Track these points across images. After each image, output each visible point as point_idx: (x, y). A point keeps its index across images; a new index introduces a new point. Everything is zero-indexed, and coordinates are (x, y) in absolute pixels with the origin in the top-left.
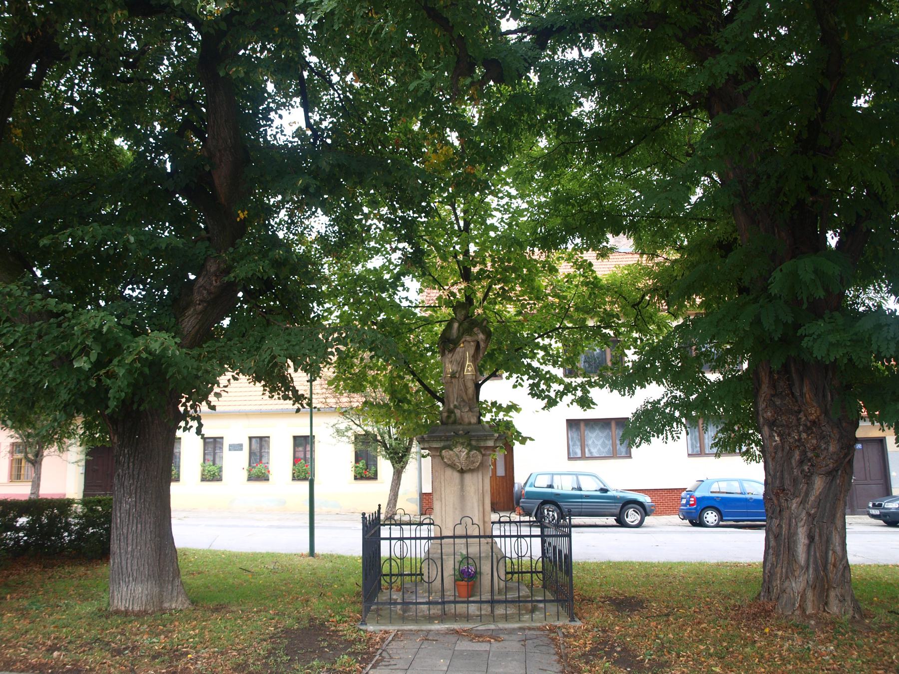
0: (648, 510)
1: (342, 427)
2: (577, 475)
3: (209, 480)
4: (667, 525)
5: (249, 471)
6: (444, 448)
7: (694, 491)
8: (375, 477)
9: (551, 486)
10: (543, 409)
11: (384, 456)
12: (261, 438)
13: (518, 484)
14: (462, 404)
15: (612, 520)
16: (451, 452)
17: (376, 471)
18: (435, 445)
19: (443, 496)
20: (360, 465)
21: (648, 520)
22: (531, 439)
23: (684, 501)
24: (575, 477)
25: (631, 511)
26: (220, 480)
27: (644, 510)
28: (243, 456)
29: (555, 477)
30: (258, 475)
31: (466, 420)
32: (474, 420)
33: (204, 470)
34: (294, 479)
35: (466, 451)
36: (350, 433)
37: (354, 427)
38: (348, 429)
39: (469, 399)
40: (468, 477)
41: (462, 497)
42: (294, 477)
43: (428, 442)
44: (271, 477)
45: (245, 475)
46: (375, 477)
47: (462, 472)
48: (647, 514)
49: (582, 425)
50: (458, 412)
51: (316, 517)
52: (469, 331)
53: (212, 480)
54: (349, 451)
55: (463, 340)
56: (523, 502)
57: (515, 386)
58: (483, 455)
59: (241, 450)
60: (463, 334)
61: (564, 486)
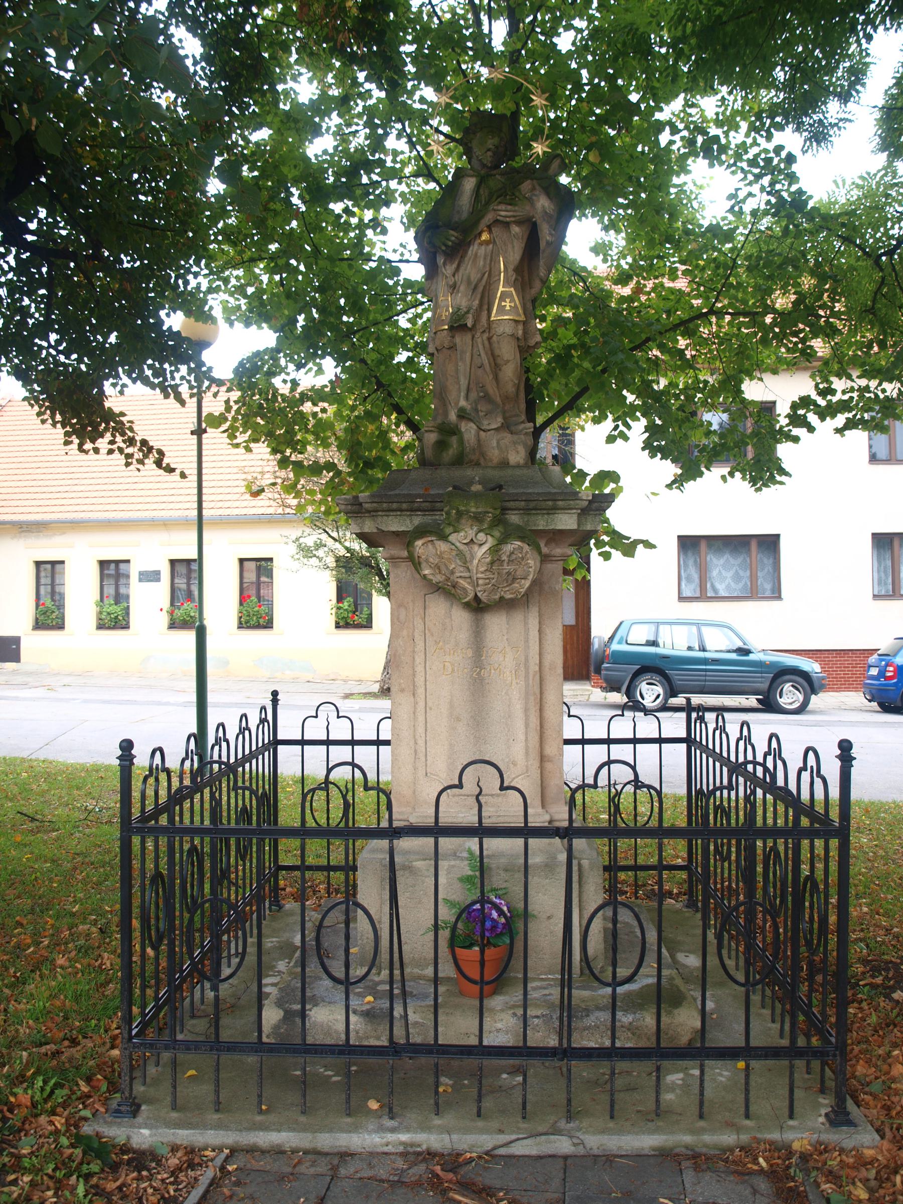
0: (816, 684)
1: (310, 541)
2: (698, 625)
3: (109, 628)
4: (840, 709)
5: (171, 613)
6: (420, 532)
7: (895, 655)
8: (367, 624)
9: (654, 643)
10: (669, 486)
11: (379, 592)
13: (600, 638)
14: (483, 407)
15: (752, 701)
16: (442, 546)
17: (371, 614)
18: (396, 524)
19: (420, 680)
20: (345, 605)
21: (815, 701)
22: (648, 545)
23: (874, 672)
24: (694, 628)
25: (787, 687)
26: (126, 627)
27: (810, 685)
28: (162, 589)
29: (661, 627)
30: (114, 619)
31: (494, 454)
32: (517, 456)
33: (101, 613)
34: (240, 626)
35: (491, 542)
36: (321, 553)
37: (330, 542)
38: (320, 545)
39: (506, 398)
41: (478, 683)
42: (240, 623)
43: (372, 513)
45: (165, 619)
46: (367, 624)
47: (477, 607)
48: (814, 691)
49: (703, 545)
50: (469, 430)
51: (194, 698)
52: (508, 192)
53: (114, 628)
54: (325, 586)
55: (489, 218)
56: (607, 669)
57: (611, 439)
58: (545, 559)
59: (158, 580)
60: (488, 203)
61: (676, 643)
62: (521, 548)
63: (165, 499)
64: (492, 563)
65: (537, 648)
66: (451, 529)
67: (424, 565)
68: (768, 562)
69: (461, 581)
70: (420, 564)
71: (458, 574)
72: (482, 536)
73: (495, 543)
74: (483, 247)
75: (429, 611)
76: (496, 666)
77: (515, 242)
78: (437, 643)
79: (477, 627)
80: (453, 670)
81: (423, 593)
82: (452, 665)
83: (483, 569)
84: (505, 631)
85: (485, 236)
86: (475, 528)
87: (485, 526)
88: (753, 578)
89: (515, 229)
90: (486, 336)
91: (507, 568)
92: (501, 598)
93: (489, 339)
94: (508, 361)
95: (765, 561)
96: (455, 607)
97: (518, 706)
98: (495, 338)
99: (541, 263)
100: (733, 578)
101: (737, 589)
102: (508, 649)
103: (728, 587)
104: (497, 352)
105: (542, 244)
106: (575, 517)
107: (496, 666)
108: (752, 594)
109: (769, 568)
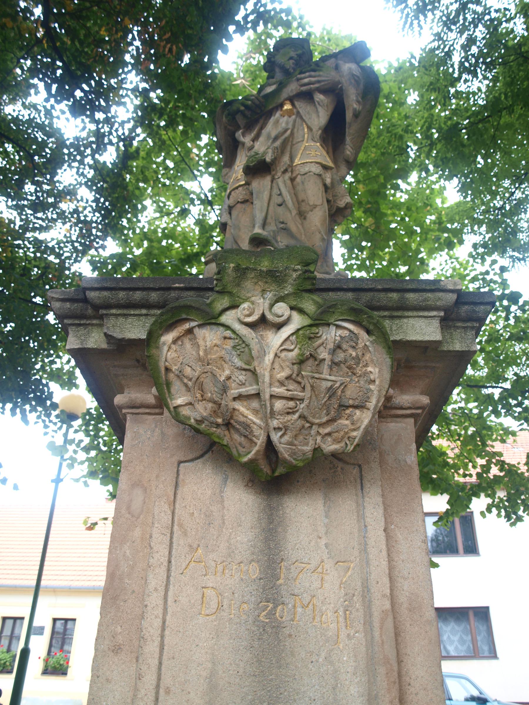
5: (46, 661)
12: (66, 620)
16: (208, 336)
40: (306, 515)
44: (70, 671)
62: (354, 337)
63: (58, 573)
64: (301, 362)
65: (384, 564)
66: (225, 302)
67: (176, 386)
68: (483, 628)
69: (240, 407)
70: (168, 384)
71: (234, 392)
72: (282, 308)
73: (307, 322)
74: (286, 118)
75: (184, 491)
76: (306, 598)
77: (320, 109)
78: (193, 549)
79: (271, 520)
80: (220, 606)
81: (175, 459)
82: (220, 594)
83: (282, 375)
84: (322, 530)
85: (287, 107)
86: (269, 295)
87: (289, 289)
88: (474, 641)
89: (319, 97)
90: (288, 175)
91: (329, 378)
92: (317, 450)
93: (292, 180)
94: (315, 206)
95: (481, 627)
96: (230, 484)
97: (354, 690)
98: (299, 179)
99: (348, 139)
100: (459, 641)
101: (463, 650)
102: (328, 565)
103: (456, 648)
104: (301, 196)
105: (349, 115)
106: (436, 323)
107: (306, 598)
108: (474, 654)
109: (484, 634)
